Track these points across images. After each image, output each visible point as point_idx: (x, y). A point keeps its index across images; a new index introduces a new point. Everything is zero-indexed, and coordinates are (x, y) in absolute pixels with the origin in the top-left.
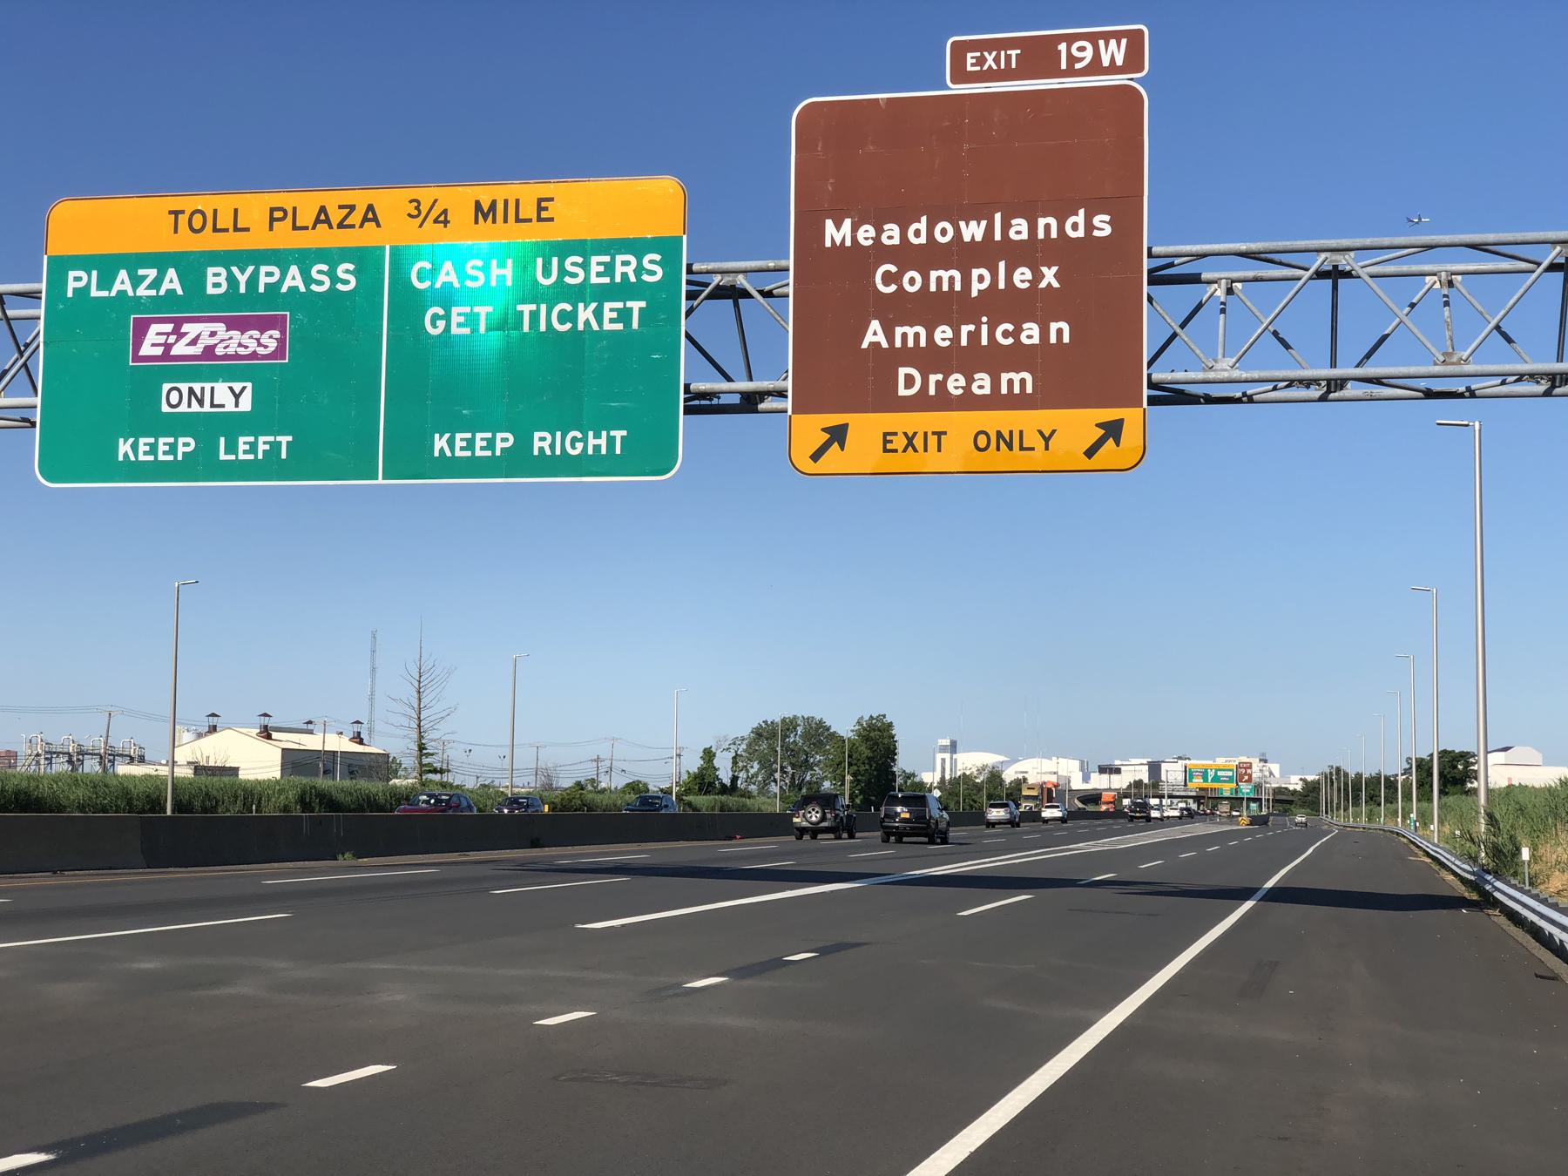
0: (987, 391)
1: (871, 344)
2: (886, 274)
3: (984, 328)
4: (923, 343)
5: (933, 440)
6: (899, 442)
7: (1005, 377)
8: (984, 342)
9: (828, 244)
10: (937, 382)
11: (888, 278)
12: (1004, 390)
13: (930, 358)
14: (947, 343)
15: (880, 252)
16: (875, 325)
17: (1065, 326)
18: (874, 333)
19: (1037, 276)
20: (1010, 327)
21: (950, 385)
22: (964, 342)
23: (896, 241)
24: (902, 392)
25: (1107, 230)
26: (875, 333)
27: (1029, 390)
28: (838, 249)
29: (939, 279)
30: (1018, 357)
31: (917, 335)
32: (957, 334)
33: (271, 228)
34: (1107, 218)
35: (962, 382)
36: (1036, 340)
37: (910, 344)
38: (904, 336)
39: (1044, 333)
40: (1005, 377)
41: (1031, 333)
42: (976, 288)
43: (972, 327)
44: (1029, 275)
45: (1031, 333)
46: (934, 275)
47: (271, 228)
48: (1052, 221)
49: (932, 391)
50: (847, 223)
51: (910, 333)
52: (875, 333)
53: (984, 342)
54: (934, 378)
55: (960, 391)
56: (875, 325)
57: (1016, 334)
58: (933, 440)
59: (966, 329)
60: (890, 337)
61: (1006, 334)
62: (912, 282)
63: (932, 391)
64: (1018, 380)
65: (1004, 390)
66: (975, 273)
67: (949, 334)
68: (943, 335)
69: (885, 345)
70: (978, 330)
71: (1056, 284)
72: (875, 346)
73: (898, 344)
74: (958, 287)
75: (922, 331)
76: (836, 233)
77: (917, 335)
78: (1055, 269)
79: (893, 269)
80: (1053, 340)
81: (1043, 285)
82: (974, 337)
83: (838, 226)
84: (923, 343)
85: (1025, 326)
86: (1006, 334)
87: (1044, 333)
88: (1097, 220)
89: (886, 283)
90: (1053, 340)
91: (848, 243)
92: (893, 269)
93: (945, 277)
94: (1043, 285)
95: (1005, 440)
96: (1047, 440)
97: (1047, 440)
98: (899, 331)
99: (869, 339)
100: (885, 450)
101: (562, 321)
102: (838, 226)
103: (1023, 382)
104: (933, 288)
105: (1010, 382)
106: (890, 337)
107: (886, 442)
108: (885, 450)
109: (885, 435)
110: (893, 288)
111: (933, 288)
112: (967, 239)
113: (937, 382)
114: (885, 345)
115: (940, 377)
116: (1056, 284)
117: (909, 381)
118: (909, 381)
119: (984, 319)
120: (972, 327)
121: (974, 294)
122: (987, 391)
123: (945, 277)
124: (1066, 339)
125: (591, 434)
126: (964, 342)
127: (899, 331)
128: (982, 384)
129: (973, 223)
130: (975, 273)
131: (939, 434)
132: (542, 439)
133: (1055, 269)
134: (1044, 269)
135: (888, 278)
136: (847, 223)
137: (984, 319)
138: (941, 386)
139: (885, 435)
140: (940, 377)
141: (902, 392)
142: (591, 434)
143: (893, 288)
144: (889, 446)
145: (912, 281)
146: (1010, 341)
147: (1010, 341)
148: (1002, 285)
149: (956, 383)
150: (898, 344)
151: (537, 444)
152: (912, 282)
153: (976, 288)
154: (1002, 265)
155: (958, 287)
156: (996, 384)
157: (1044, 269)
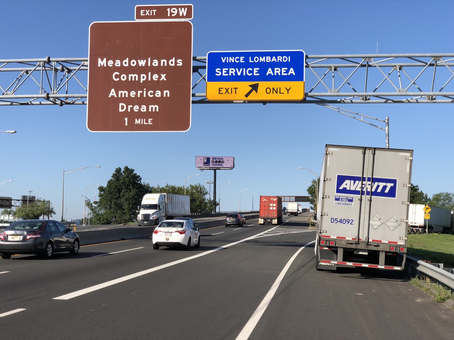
3: (145, 92)
4: (127, 96)
5: (234, 90)
6: (224, 91)
7: (150, 106)
8: (145, 96)
9: (99, 66)
10: (131, 108)
11: (117, 76)
13: (129, 101)
14: (134, 96)
15: (115, 68)
16: (113, 90)
17: (168, 92)
18: (113, 93)
19: (160, 77)
20: (152, 92)
22: (139, 96)
23: (119, 65)
25: (181, 64)
26: (113, 93)
28: (102, 67)
30: (154, 101)
32: (137, 93)
34: (181, 60)
35: (138, 108)
36: (160, 96)
37: (123, 96)
39: (162, 94)
40: (150, 106)
41: (158, 94)
42: (142, 80)
43: (141, 92)
44: (157, 77)
45: (158, 94)
46: (130, 76)
48: (165, 61)
49: (129, 111)
50: (105, 59)
51: (123, 93)
52: (113, 93)
53: (145, 96)
54: (130, 107)
56: (113, 90)
57: (154, 94)
58: (234, 90)
59: (139, 92)
60: (117, 94)
61: (151, 94)
62: (124, 77)
63: (129, 111)
64: (154, 108)
66: (142, 75)
67: (135, 93)
68: (133, 94)
69: (116, 96)
70: (143, 92)
71: (165, 79)
72: (113, 96)
73: (120, 96)
74: (137, 79)
76: (101, 62)
77: (125, 94)
78: (165, 75)
79: (118, 74)
81: (161, 79)
82: (142, 94)
83: (102, 61)
84: (127, 96)
85: (157, 92)
86: (151, 94)
87: (162, 94)
88: (178, 61)
89: (116, 78)
90: (165, 96)
91: (105, 66)
92: (118, 74)
93: (133, 76)
94: (161, 79)
95: (275, 91)
96: (288, 91)
97: (288, 91)
98: (120, 92)
100: (219, 93)
101: (116, 78)
102: (102, 61)
103: (156, 108)
104: (130, 80)
105: (152, 108)
106: (117, 94)
107: (219, 91)
108: (219, 93)
109: (219, 88)
110: (118, 79)
111: (130, 80)
112: (140, 65)
114: (116, 96)
115: (131, 106)
116: (165, 79)
117: (123, 107)
118: (123, 107)
119: (145, 89)
120: (141, 92)
123: (133, 76)
126: (139, 96)
127: (120, 92)
128: (144, 108)
129: (142, 61)
130: (142, 75)
131: (236, 88)
132: (277, 70)
133: (165, 75)
134: (162, 75)
135: (117, 76)
136: (105, 59)
137: (145, 89)
138: (132, 109)
139: (219, 88)
140: (131, 106)
143: (118, 79)
144: (220, 92)
145: (124, 77)
146: (152, 96)
147: (152, 96)
148: (149, 79)
149: (136, 108)
150: (120, 96)
152: (124, 77)
153: (142, 80)
154: (150, 73)
155: (137, 79)
156: (148, 109)
157: (162, 75)
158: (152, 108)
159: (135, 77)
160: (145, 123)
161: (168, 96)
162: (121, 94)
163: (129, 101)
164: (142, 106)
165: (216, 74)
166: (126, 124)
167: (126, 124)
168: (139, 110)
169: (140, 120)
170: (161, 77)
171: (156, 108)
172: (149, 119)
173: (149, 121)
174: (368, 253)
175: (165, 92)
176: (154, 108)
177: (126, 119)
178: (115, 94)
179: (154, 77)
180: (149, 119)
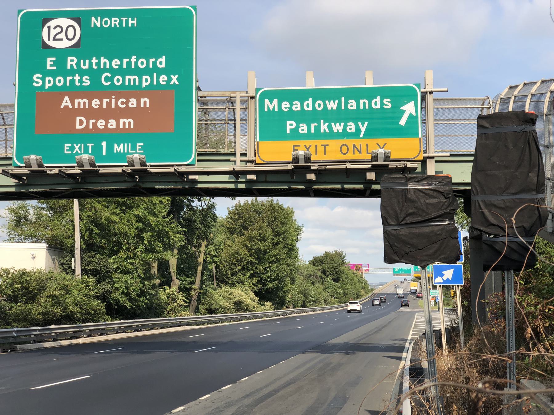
0: (114, 127)
1: (65, 106)
2: (106, 77)
3: (113, 101)
4: (87, 106)
7: (122, 121)
8: (113, 106)
11: (107, 79)
12: (121, 127)
13: (89, 113)
14: (97, 107)
16: (67, 98)
17: (147, 100)
18: (66, 102)
19: (170, 79)
20: (124, 100)
21: (99, 124)
22: (105, 106)
24: (78, 127)
26: (66, 102)
27: (132, 126)
29: (129, 80)
30: (127, 112)
31: (84, 103)
33: (322, 145)
34: (88, 78)
35: (104, 123)
36: (135, 106)
37: (82, 107)
38: (79, 103)
39: (139, 103)
40: (122, 121)
42: (144, 84)
43: (108, 100)
44: (166, 79)
47: (322, 145)
49: (91, 127)
51: (81, 102)
52: (66, 102)
53: (113, 106)
54: (91, 121)
55: (103, 127)
56: (67, 98)
57: (127, 103)
59: (105, 101)
60: (73, 103)
61: (122, 103)
63: (91, 127)
64: (127, 122)
65: (121, 127)
67: (98, 103)
68: (95, 103)
69: (71, 107)
70: (111, 101)
71: (177, 83)
73: (76, 107)
74: (137, 83)
75: (87, 101)
77: (84, 103)
78: (177, 76)
79: (109, 75)
80: (142, 106)
81: (172, 83)
82: (108, 104)
84: (87, 106)
85: (131, 100)
86: (122, 103)
87: (139, 103)
89: (106, 81)
90: (142, 106)
92: (109, 75)
93: (132, 79)
94: (172, 83)
98: (77, 101)
99: (64, 104)
101: (106, 81)
103: (129, 123)
104: (127, 83)
106: (73, 103)
110: (109, 83)
111: (127, 83)
113: (93, 123)
114: (71, 107)
115: (94, 121)
116: (177, 83)
117: (81, 123)
118: (81, 123)
119: (113, 97)
120: (108, 100)
121: (143, 86)
122: (114, 127)
123: (132, 79)
124: (148, 106)
125: (130, 19)
126: (105, 106)
127: (77, 101)
133: (177, 76)
134: (172, 76)
135: (107, 79)
137: (113, 97)
138: (95, 125)
140: (94, 121)
141: (78, 127)
142: (130, 19)
143: (109, 83)
145: (118, 80)
146: (124, 106)
147: (124, 106)
148: (155, 83)
149: (101, 124)
150: (76, 107)
151: (69, 63)
152: (118, 80)
154: (155, 75)
155: (137, 83)
157: (172, 76)
158: (124, 123)
159: (135, 80)
160: (130, 151)
161: (148, 106)
162: (79, 103)
163: (89, 113)
164: (110, 121)
165: (35, 84)
166: (104, 153)
167: (104, 153)
168: (106, 126)
169: (122, 145)
170: (171, 79)
171: (129, 123)
172: (138, 144)
173: (138, 148)
174: (76, 198)
175: (143, 100)
176: (127, 122)
177: (104, 144)
178: (69, 104)
179: (161, 79)
180: (138, 144)
